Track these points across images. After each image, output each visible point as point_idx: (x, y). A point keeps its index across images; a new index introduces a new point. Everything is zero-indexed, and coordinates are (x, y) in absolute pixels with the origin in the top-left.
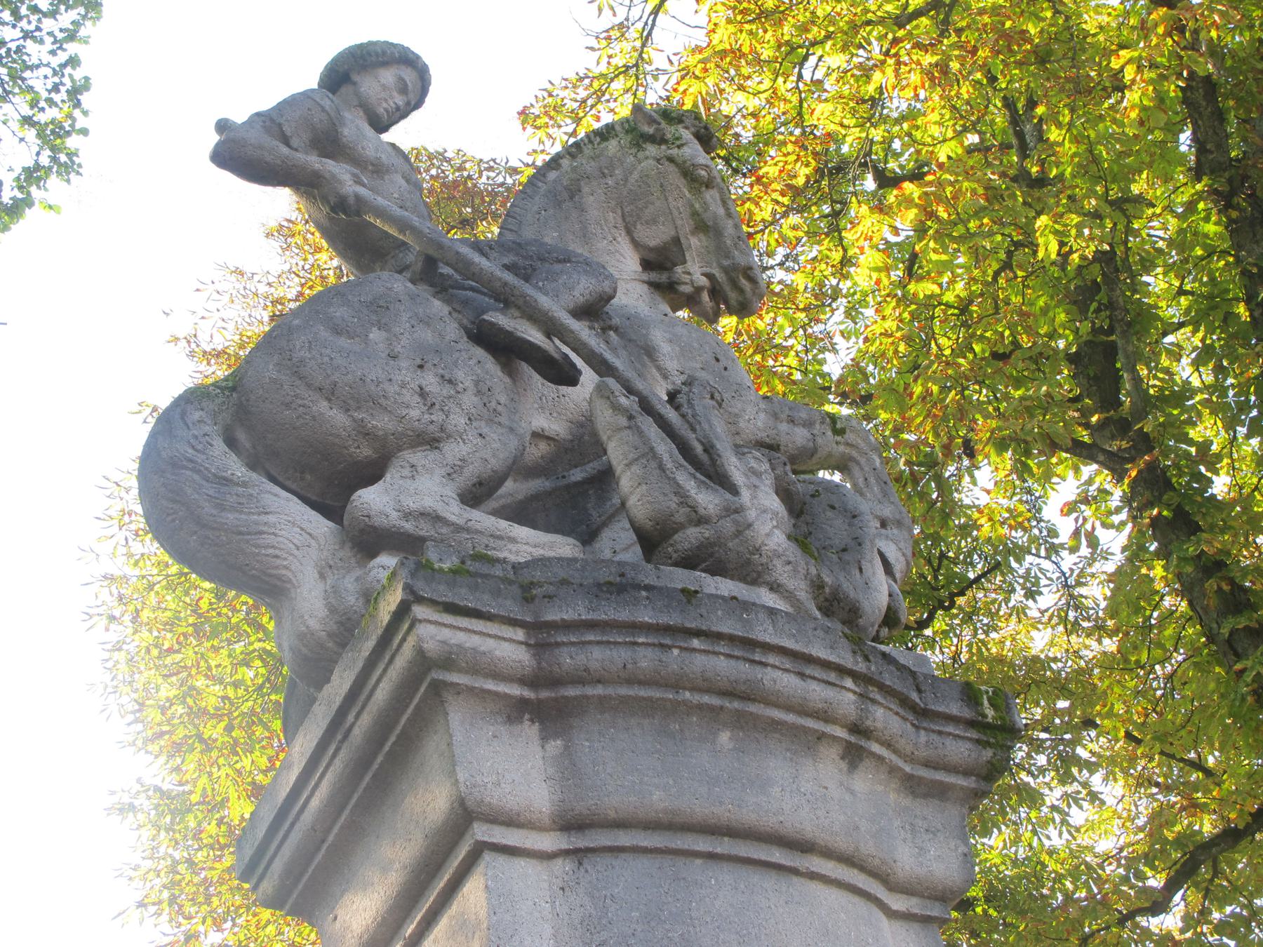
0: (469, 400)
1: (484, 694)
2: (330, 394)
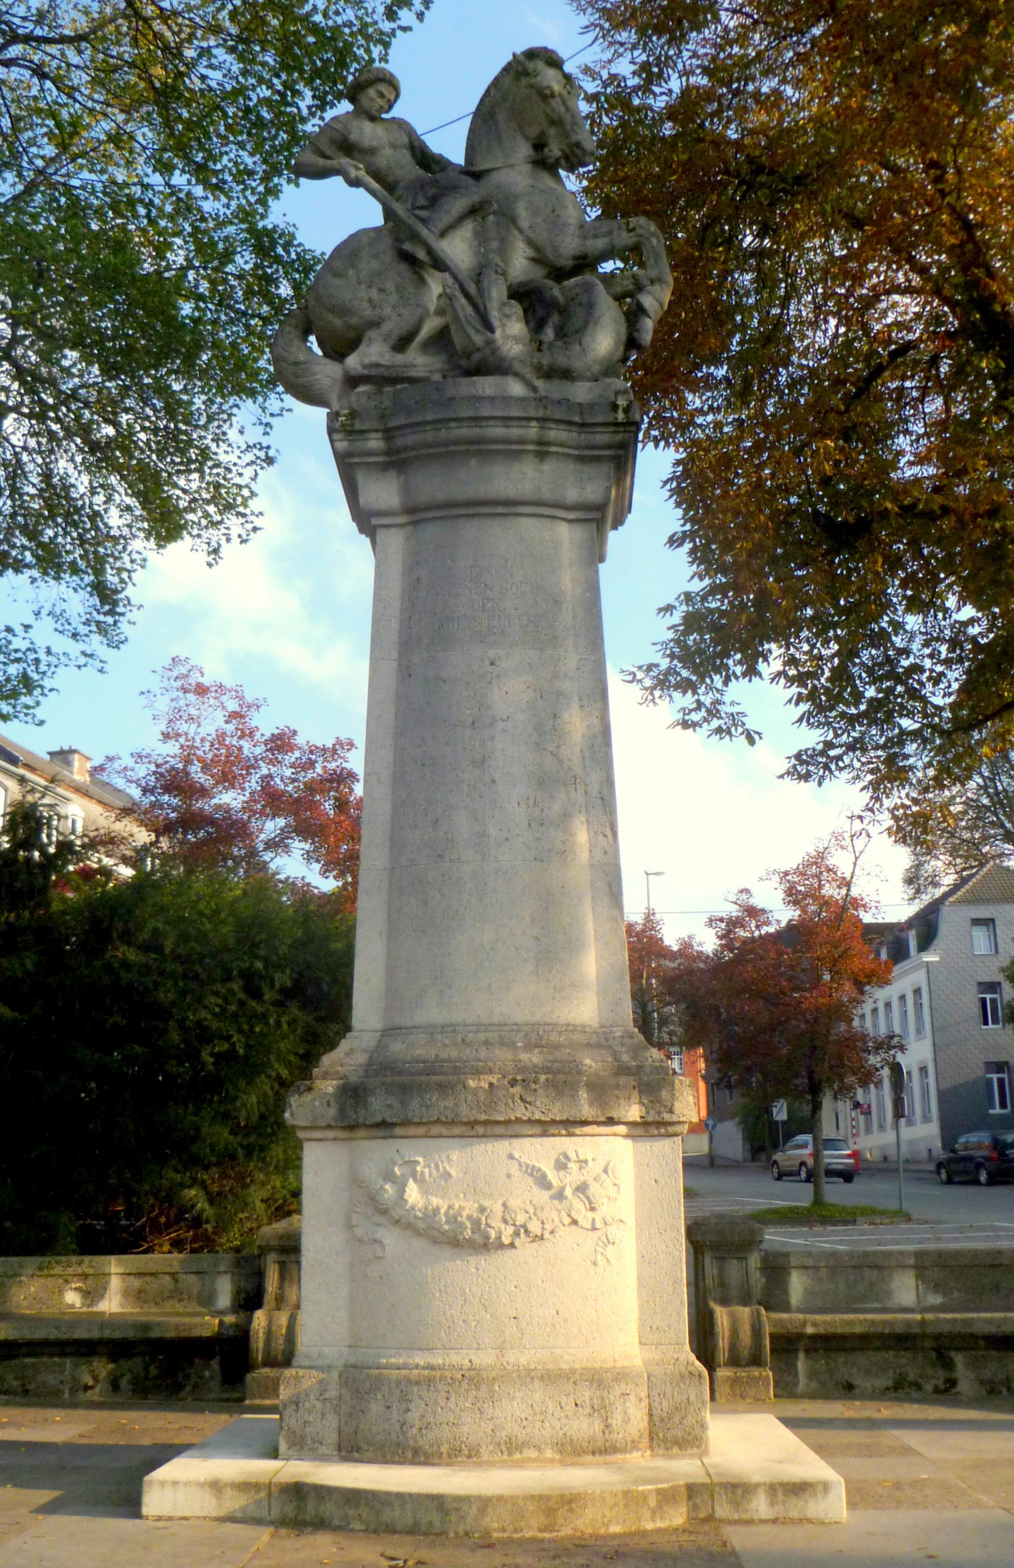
0: (394, 298)
1: (368, 464)
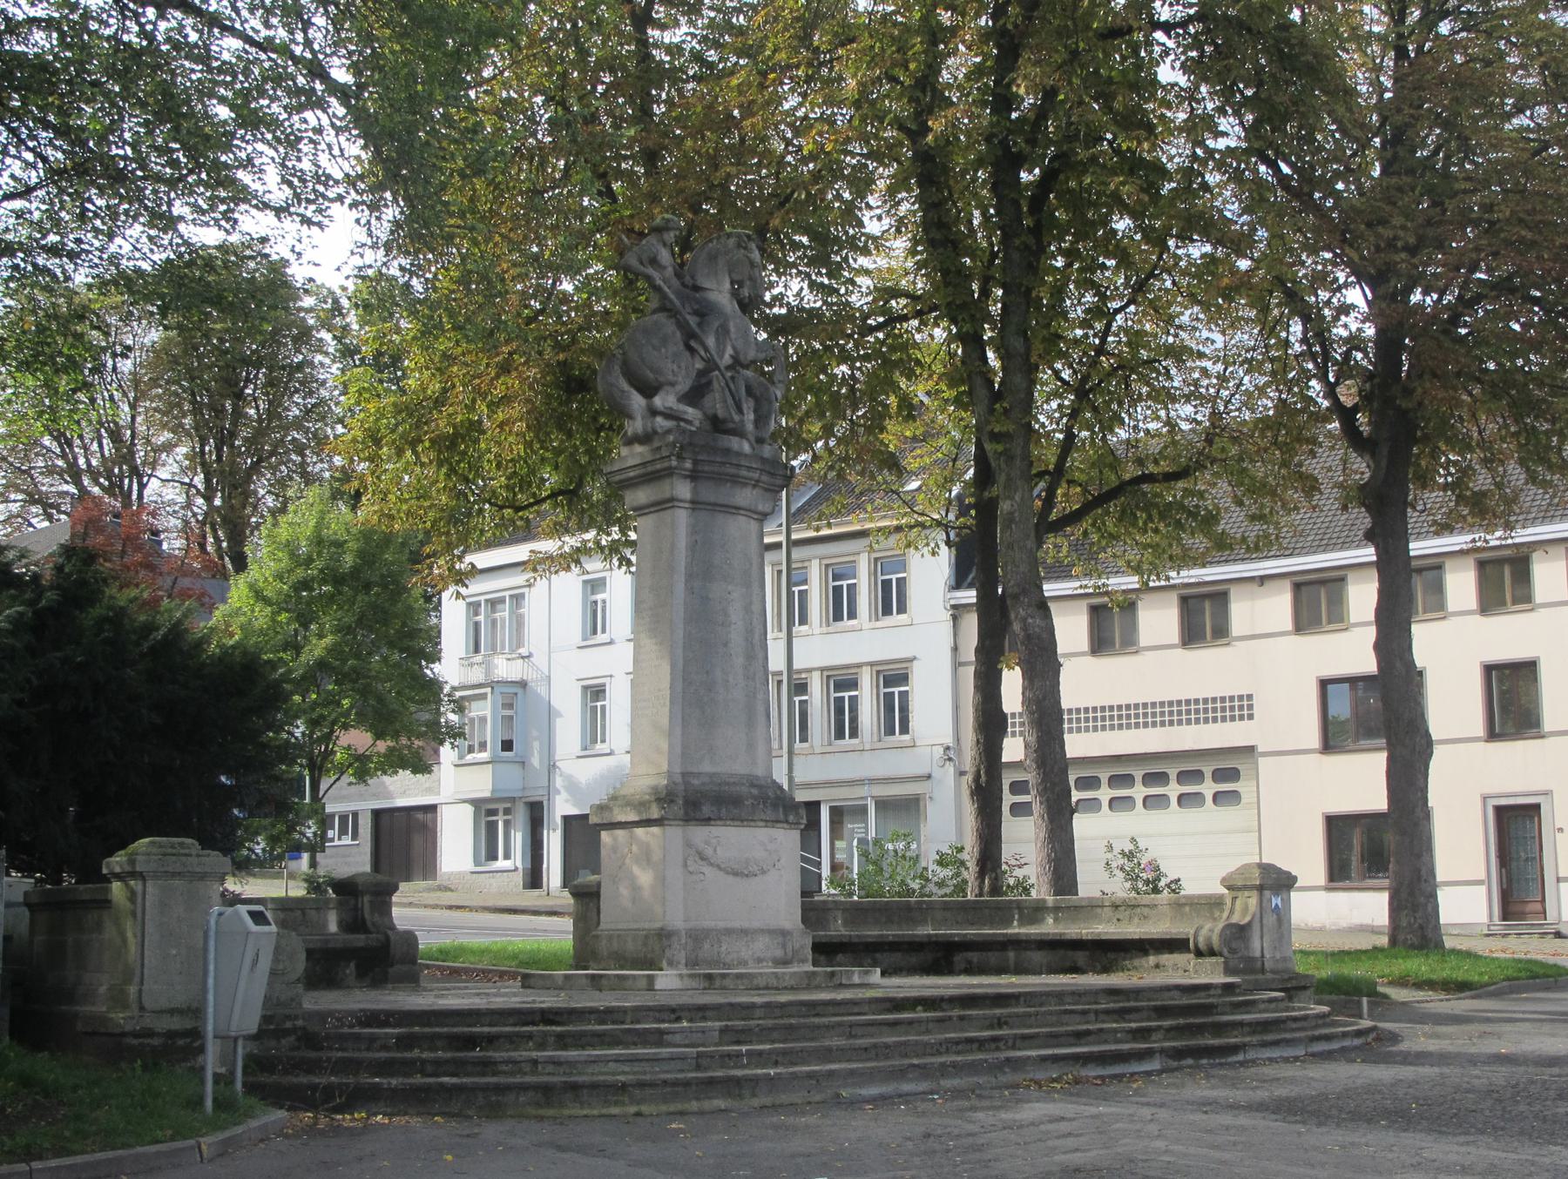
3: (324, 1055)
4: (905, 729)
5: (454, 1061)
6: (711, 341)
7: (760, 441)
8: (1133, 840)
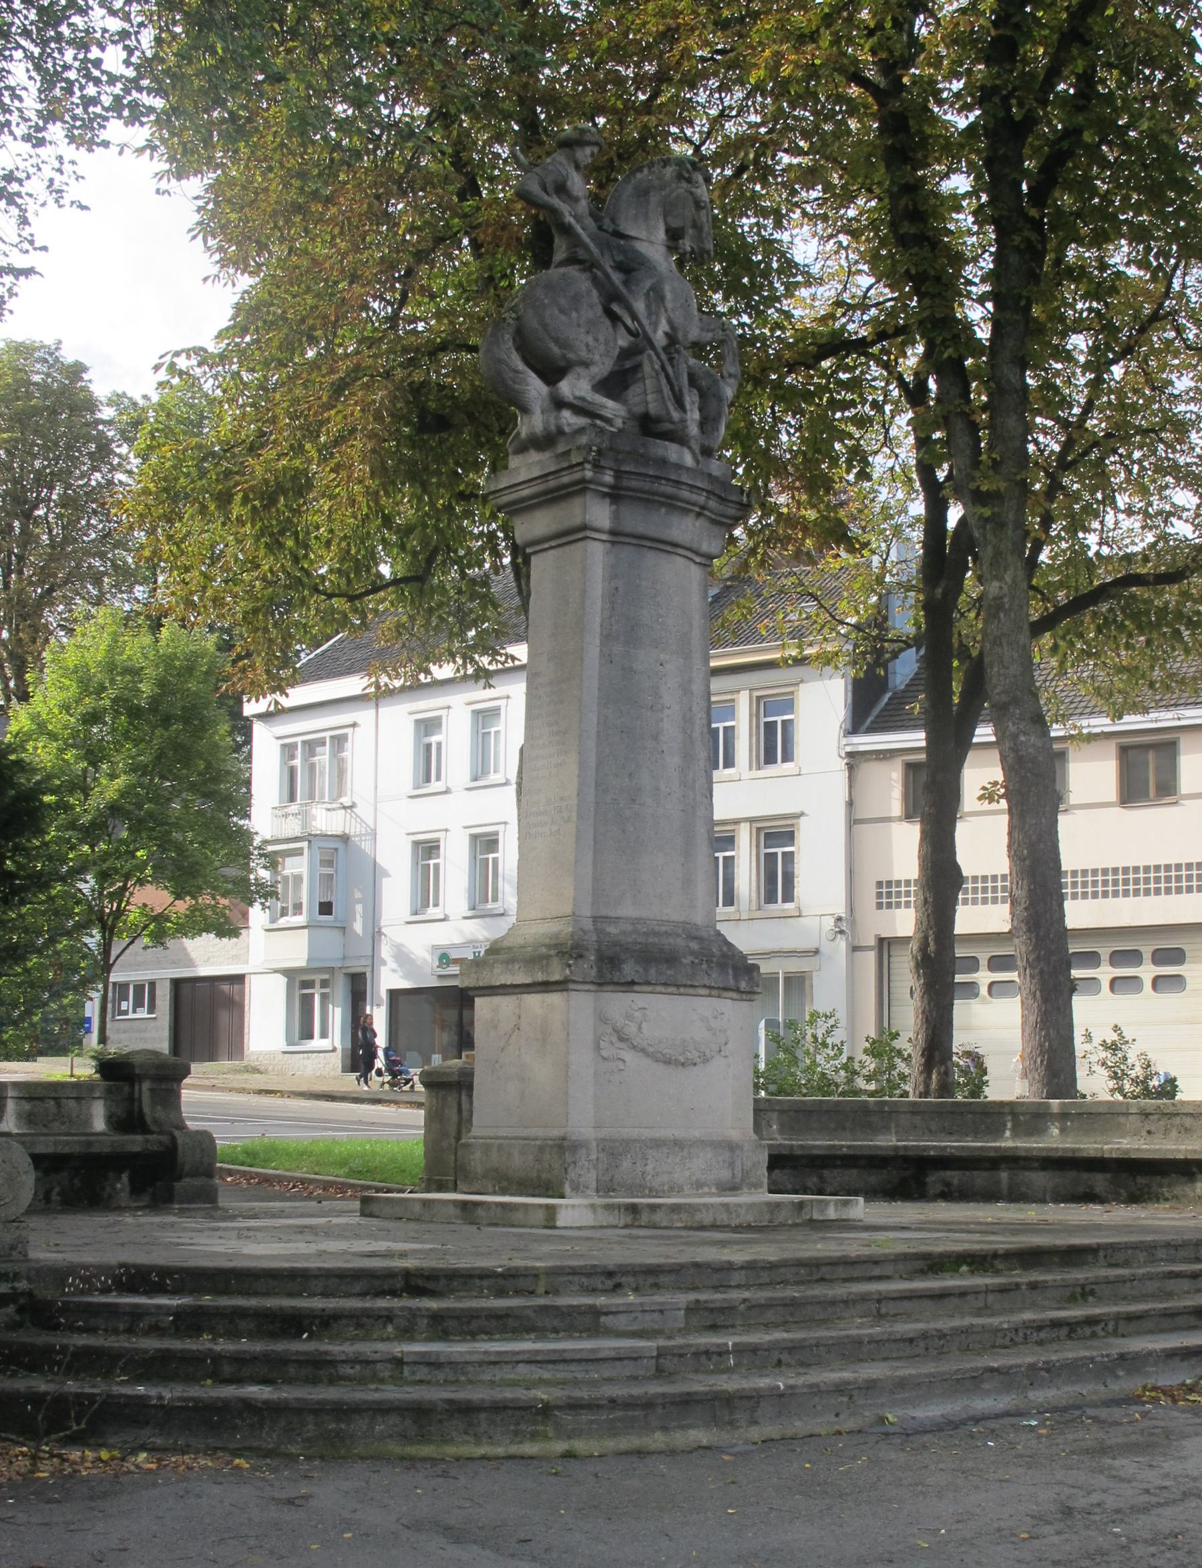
0: (602, 347)
2: (556, 341)
3: (57, 1340)
4: (788, 897)
5: (267, 1358)
6: (640, 306)
7: (707, 452)
8: (1116, 1028)
